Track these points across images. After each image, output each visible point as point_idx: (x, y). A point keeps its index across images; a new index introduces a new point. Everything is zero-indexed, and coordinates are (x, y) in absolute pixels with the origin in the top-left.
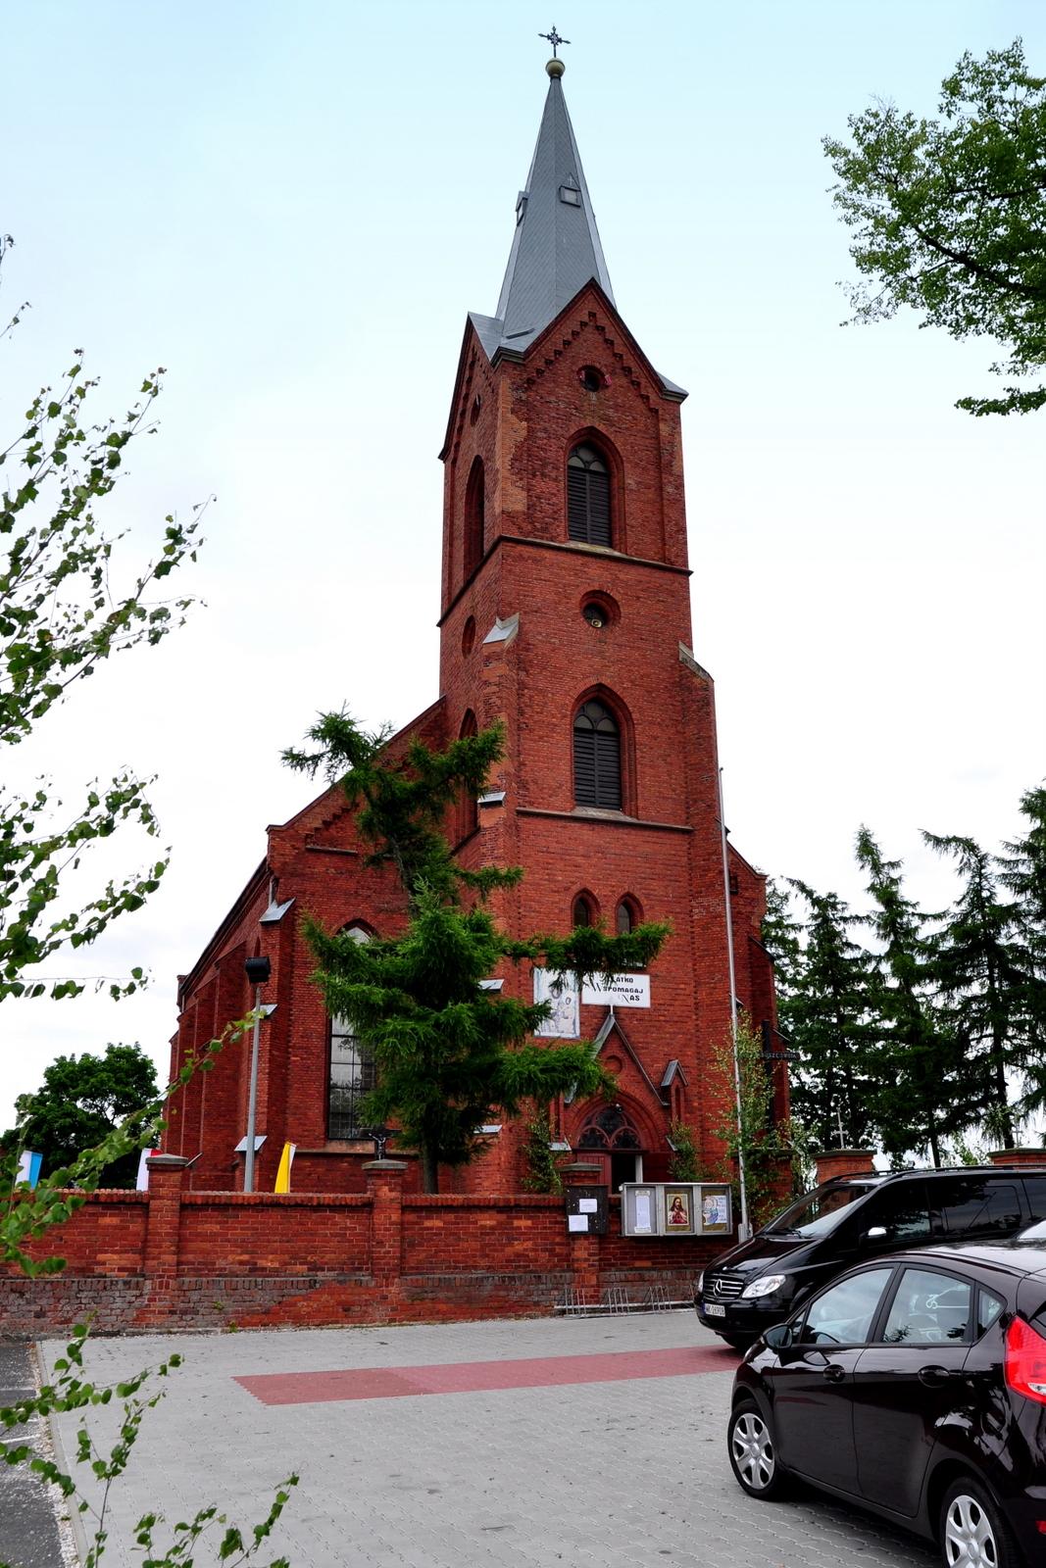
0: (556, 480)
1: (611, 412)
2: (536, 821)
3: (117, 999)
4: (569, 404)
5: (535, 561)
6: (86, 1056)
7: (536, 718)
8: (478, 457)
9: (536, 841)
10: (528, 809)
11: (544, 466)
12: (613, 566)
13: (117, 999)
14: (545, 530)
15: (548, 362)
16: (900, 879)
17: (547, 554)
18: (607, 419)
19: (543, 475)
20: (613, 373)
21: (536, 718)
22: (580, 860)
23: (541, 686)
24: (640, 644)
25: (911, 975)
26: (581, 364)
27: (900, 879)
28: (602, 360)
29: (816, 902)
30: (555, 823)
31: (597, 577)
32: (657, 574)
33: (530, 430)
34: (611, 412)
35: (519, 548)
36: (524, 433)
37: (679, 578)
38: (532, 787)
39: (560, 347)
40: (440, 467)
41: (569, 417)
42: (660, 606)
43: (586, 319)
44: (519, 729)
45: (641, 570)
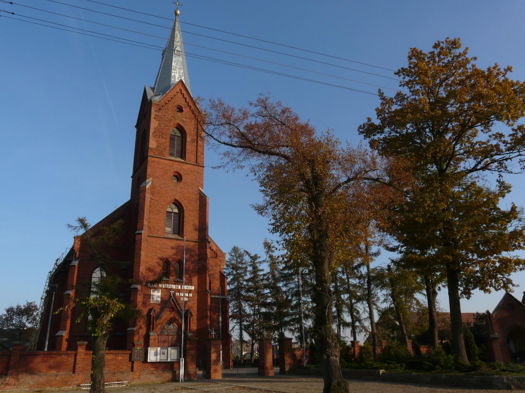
0: (166, 139)
1: (184, 119)
2: (153, 238)
3: (398, 73)
4: (171, 116)
5: (158, 162)
6: (18, 306)
7: (155, 208)
8: (145, 130)
9: (155, 245)
10: (151, 235)
11: (163, 134)
12: (182, 164)
13: (398, 73)
14: (161, 153)
15: (166, 104)
16: (513, 209)
17: (162, 160)
18: (183, 121)
19: (162, 137)
20: (186, 107)
21: (155, 208)
22: (165, 250)
23: (157, 199)
24: (188, 187)
25: (277, 280)
26: (176, 104)
27: (513, 209)
28: (183, 103)
29: (251, 257)
30: (158, 239)
31: (177, 167)
32: (194, 167)
33: (159, 124)
34: (184, 119)
35: (154, 159)
36: (157, 125)
37: (201, 168)
38: (152, 228)
39: (170, 99)
40: (135, 129)
41: (171, 120)
42: (194, 176)
43: (179, 91)
44: (150, 212)
45: (189, 165)
